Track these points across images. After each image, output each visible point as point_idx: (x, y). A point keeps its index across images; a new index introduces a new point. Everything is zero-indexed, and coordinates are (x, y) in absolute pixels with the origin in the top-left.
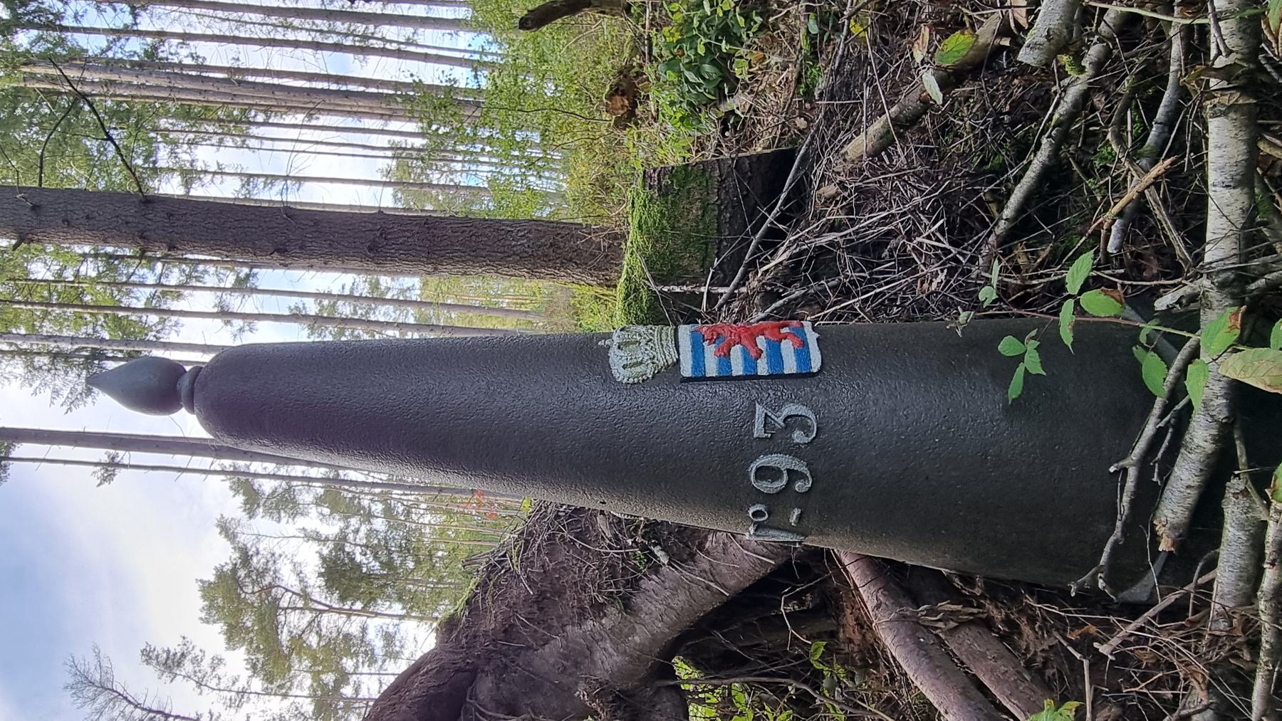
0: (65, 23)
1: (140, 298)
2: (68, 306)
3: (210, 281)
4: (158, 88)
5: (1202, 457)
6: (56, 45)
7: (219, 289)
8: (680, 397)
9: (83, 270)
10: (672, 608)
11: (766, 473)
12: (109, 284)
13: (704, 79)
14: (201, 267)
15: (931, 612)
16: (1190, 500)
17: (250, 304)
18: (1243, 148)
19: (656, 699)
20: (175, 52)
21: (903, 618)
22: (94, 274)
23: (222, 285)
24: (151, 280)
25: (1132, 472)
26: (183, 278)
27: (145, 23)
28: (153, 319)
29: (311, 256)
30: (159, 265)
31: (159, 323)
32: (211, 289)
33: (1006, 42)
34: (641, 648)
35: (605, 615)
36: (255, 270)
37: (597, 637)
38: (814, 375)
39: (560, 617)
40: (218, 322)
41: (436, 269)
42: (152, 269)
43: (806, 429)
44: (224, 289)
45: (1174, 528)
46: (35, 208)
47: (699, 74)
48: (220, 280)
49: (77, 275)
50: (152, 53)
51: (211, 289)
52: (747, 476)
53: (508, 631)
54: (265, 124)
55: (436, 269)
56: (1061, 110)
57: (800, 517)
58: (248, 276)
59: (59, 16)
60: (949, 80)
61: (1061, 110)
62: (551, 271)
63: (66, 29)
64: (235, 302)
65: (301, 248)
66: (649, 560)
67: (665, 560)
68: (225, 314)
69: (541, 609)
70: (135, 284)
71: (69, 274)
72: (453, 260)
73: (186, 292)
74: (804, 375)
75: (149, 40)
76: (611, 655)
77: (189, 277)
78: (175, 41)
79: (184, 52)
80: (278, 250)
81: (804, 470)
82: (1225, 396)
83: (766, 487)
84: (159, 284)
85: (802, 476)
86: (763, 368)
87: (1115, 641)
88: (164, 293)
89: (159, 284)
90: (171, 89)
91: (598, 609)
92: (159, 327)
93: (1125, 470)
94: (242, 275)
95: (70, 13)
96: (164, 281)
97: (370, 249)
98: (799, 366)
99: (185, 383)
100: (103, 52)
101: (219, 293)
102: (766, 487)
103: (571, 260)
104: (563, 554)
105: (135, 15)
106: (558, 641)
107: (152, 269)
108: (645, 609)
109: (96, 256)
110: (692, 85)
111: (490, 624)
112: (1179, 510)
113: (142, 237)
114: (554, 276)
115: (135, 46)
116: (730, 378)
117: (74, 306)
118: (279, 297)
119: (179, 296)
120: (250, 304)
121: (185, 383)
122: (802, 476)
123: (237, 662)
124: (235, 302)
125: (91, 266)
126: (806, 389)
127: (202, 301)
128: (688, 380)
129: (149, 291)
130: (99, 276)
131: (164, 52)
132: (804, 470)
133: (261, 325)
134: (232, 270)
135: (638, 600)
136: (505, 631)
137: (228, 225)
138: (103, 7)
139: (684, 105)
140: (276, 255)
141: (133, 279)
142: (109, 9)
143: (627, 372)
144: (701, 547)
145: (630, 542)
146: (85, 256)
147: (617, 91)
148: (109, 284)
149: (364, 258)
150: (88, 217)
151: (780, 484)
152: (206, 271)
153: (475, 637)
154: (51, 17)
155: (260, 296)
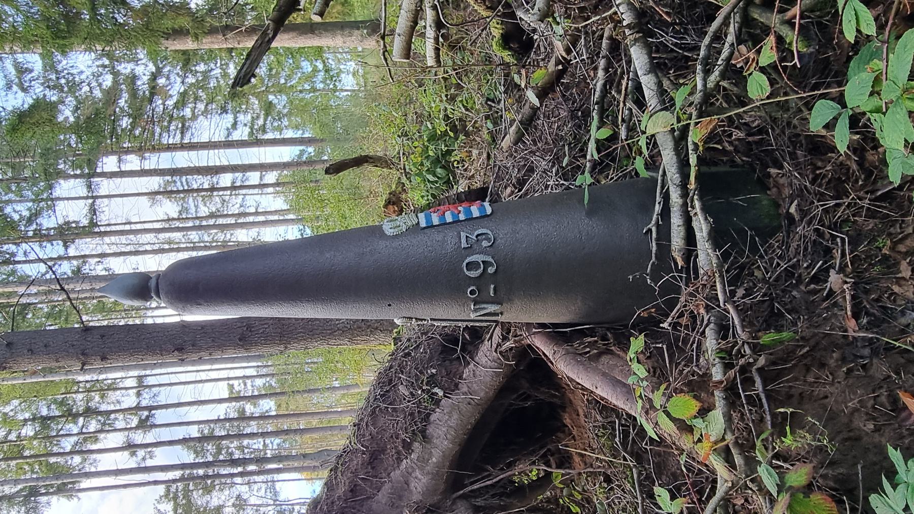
0: (17, 259)
1: (67, 444)
2: (12, 459)
3: (120, 424)
4: (83, 291)
5: (679, 207)
6: (9, 276)
7: (126, 429)
8: (421, 238)
9: (23, 432)
10: (451, 427)
11: (471, 266)
12: (43, 438)
13: (438, 178)
14: (113, 416)
15: (580, 344)
16: (682, 233)
17: (150, 437)
18: (646, 56)
19: (454, 507)
20: (96, 268)
21: (568, 353)
22: (32, 434)
23: (129, 426)
24: (75, 430)
25: (654, 229)
26: (99, 427)
27: (72, 252)
28: (77, 459)
29: (200, 349)
30: (81, 420)
31: (81, 463)
32: (120, 430)
33: (560, 67)
34: (439, 466)
35: (413, 451)
36: (153, 412)
37: (410, 470)
38: (488, 216)
39: (386, 470)
40: (126, 454)
41: (286, 347)
42: (76, 423)
43: (489, 240)
44: (131, 429)
45: (679, 251)
46: (9, 345)
47: (435, 175)
48: (127, 423)
49: (19, 437)
50: (77, 272)
51: (120, 430)
52: (462, 269)
53: (354, 490)
54: (157, 308)
55: (286, 347)
56: (596, 96)
57: (495, 289)
58: (148, 417)
59: (13, 255)
60: (543, 94)
61: (596, 96)
62: (365, 338)
63: (19, 262)
64: (139, 437)
65: (193, 346)
66: (433, 399)
67: (441, 393)
68: (131, 447)
69: (373, 468)
70: (63, 435)
71: (13, 437)
72: (298, 340)
73: (102, 436)
74: (484, 217)
75: (75, 263)
76: (420, 480)
77: (104, 424)
78: (93, 261)
79: (100, 267)
80: (177, 350)
81: (491, 260)
82: (677, 173)
83: (473, 274)
84: (81, 433)
85: (491, 264)
86: (462, 217)
87: (669, 320)
88: (85, 440)
89: (81, 433)
90: (92, 290)
91: (408, 446)
92: (81, 466)
93: (650, 230)
94: (143, 417)
95: (21, 252)
96: (84, 430)
97: (240, 340)
98: (480, 212)
99: (153, 283)
100: (43, 275)
101: (126, 433)
102: (473, 274)
103: (377, 328)
104: (381, 421)
105: (66, 247)
106: (387, 487)
107: (76, 423)
108: (435, 435)
109: (34, 419)
110: (432, 182)
111: (341, 490)
112: (679, 240)
113: (83, 354)
114: (366, 341)
115: (65, 268)
116: (446, 224)
117: (15, 458)
118: (172, 428)
119: (96, 440)
120: (150, 437)
121: (153, 283)
122: (491, 264)
123: (231, 82)
124: (139, 437)
125: (30, 428)
126: (485, 221)
127: (114, 440)
128: (425, 228)
129: (73, 440)
130: (36, 434)
131: (86, 269)
132: (491, 260)
133: (158, 451)
134: (136, 414)
135: (430, 430)
136: (352, 491)
137: (143, 337)
138: (44, 244)
139: (430, 197)
140: (176, 353)
141: (61, 433)
142: (49, 245)
143: (392, 230)
144: (461, 378)
145: (420, 392)
146: (25, 420)
147: (389, 202)
148: (43, 438)
149: (236, 346)
150: (46, 346)
151: (480, 271)
152: (116, 419)
153: (333, 503)
154: (8, 256)
155: (157, 430)
